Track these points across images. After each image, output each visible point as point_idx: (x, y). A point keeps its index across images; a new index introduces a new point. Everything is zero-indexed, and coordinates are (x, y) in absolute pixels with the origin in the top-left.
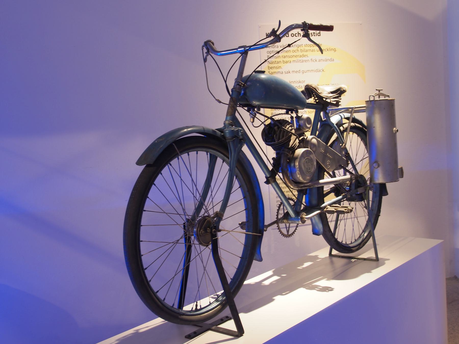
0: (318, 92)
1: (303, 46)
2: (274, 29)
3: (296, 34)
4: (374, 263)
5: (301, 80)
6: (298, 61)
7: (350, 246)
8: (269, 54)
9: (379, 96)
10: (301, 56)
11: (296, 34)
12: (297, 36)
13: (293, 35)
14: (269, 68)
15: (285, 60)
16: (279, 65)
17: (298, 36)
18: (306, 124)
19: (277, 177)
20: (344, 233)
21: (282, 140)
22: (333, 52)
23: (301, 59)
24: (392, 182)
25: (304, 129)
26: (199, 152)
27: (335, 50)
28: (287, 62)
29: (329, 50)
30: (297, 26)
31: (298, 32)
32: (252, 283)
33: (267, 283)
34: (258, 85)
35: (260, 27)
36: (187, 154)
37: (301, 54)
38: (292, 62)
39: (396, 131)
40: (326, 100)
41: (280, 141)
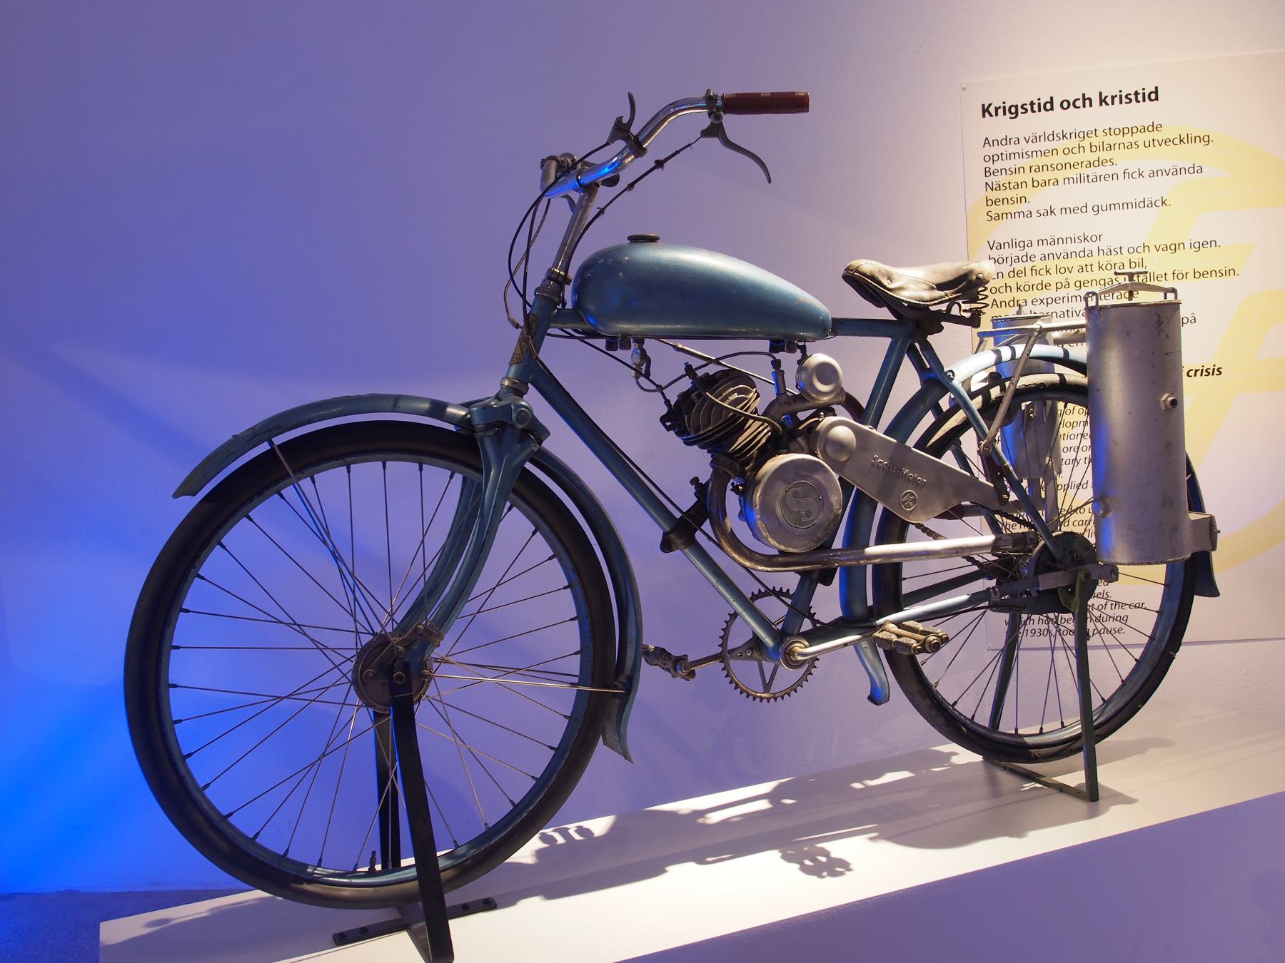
0: (885, 287)
1: (1100, 133)
2: (619, 120)
3: (1079, 99)
4: (1081, 806)
5: (1088, 234)
6: (1080, 179)
7: (1025, 742)
8: (990, 164)
9: (1131, 294)
10: (1090, 164)
11: (1079, 99)
12: (1079, 107)
13: (1065, 105)
14: (990, 203)
15: (1040, 176)
16: (1020, 192)
17: (1084, 106)
18: (812, 385)
19: (699, 536)
21: (705, 431)
22: (1199, 145)
23: (1091, 171)
24: (1149, 564)
25: (813, 398)
27: (1207, 140)
28: (1046, 183)
29: (1185, 140)
30: (689, 103)
31: (1084, 95)
32: (682, 812)
33: (714, 818)
34: (621, 274)
35: (964, 89)
37: (1092, 157)
38: (1061, 182)
39: (1168, 403)
41: (701, 432)
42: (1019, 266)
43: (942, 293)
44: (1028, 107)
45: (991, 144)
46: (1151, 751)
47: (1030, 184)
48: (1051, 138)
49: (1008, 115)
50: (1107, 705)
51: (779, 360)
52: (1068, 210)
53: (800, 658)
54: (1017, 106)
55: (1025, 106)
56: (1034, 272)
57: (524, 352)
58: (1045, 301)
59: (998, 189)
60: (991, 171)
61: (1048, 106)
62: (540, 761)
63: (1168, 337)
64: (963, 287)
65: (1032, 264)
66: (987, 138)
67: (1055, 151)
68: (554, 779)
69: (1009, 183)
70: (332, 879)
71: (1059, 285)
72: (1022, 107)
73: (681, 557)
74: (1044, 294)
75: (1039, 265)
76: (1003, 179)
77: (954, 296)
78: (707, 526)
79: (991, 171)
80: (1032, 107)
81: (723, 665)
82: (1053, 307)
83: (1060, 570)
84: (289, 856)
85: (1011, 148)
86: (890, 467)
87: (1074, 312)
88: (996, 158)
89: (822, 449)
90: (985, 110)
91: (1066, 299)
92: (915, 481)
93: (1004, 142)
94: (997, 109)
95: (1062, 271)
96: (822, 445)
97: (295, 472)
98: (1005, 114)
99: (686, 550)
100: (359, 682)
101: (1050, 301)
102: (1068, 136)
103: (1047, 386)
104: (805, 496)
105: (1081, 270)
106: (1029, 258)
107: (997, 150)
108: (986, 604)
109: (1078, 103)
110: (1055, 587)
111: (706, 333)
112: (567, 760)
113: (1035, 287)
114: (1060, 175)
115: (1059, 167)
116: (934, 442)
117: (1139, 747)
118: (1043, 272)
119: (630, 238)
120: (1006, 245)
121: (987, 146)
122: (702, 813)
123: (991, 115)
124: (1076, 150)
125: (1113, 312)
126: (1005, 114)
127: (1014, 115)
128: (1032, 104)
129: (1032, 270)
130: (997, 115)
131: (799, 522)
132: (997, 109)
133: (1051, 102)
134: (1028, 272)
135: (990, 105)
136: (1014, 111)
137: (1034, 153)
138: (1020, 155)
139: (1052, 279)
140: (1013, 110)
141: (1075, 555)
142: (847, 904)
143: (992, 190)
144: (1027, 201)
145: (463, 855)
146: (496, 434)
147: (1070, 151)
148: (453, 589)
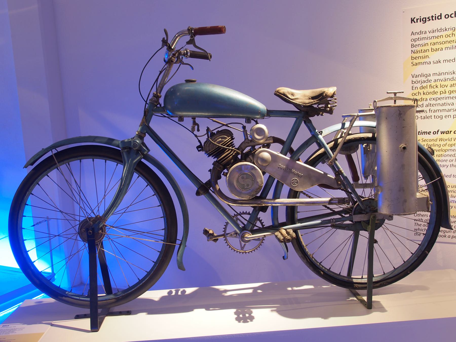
3: (453, 14)
9: (395, 101)
11: (453, 14)
12: (453, 17)
13: (447, 16)
15: (434, 47)
16: (426, 54)
18: (254, 136)
20: (68, 184)
26: (140, 177)
28: (437, 50)
31: (210, 61)
33: (229, 294)
34: (178, 94)
35: (404, 12)
36: (92, 160)
38: (444, 49)
40: (148, 104)
42: (424, 85)
43: (313, 101)
44: (431, 18)
45: (414, 34)
46: (417, 291)
47: (430, 50)
48: (440, 31)
49: (422, 22)
50: (395, 270)
51: (245, 126)
52: (447, 61)
53: (247, 239)
54: (426, 18)
55: (429, 18)
56: (431, 87)
57: (143, 122)
58: (435, 99)
59: (417, 53)
60: (414, 46)
61: (439, 17)
62: (149, 266)
63: (404, 120)
64: (320, 98)
65: (430, 83)
66: (413, 32)
67: (441, 36)
68: (152, 273)
69: (422, 50)
70: (73, 297)
71: (441, 93)
72: (428, 18)
73: (203, 197)
74: (435, 96)
75: (433, 84)
76: (419, 48)
77: (317, 102)
78: (211, 188)
79: (414, 46)
80: (433, 18)
81: (224, 239)
82: (439, 102)
83: (363, 214)
84: (341, 274)
85: (423, 36)
86: (286, 169)
87: (448, 104)
88: (416, 40)
89: (256, 161)
90: (412, 20)
91: (444, 98)
92: (298, 175)
93: (420, 33)
94: (417, 20)
95: (443, 86)
96: (256, 159)
97: (58, 162)
98: (420, 21)
99: (205, 195)
100: (80, 233)
101: (437, 99)
102: (447, 30)
103: (365, 138)
104: (247, 178)
105: (451, 86)
106: (429, 81)
107: (417, 36)
108: (330, 225)
109: (452, 16)
110: (361, 220)
111: (217, 116)
112: (416, 254)
113: (431, 93)
114: (443, 46)
115: (443, 43)
116: (311, 160)
117: (410, 289)
118: (435, 87)
119: (185, 81)
120: (419, 76)
121: (413, 35)
122: (226, 291)
123: (415, 22)
124: (451, 36)
125: (384, 109)
126: (420, 21)
127: (424, 22)
128: (432, 17)
129: (430, 86)
130: (417, 22)
131: (243, 188)
132: (417, 20)
133: (441, 16)
134: (428, 87)
135: (414, 18)
136: (424, 20)
137: (433, 37)
138: (427, 38)
139: (439, 90)
140: (424, 20)
141: (371, 208)
142: (237, 334)
143: (414, 53)
144: (429, 58)
145: (119, 295)
146: (128, 151)
147: (449, 36)
148: (111, 204)
